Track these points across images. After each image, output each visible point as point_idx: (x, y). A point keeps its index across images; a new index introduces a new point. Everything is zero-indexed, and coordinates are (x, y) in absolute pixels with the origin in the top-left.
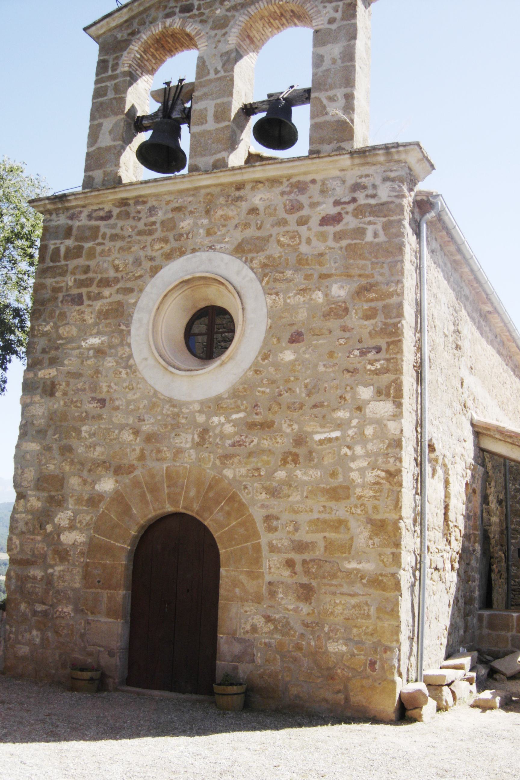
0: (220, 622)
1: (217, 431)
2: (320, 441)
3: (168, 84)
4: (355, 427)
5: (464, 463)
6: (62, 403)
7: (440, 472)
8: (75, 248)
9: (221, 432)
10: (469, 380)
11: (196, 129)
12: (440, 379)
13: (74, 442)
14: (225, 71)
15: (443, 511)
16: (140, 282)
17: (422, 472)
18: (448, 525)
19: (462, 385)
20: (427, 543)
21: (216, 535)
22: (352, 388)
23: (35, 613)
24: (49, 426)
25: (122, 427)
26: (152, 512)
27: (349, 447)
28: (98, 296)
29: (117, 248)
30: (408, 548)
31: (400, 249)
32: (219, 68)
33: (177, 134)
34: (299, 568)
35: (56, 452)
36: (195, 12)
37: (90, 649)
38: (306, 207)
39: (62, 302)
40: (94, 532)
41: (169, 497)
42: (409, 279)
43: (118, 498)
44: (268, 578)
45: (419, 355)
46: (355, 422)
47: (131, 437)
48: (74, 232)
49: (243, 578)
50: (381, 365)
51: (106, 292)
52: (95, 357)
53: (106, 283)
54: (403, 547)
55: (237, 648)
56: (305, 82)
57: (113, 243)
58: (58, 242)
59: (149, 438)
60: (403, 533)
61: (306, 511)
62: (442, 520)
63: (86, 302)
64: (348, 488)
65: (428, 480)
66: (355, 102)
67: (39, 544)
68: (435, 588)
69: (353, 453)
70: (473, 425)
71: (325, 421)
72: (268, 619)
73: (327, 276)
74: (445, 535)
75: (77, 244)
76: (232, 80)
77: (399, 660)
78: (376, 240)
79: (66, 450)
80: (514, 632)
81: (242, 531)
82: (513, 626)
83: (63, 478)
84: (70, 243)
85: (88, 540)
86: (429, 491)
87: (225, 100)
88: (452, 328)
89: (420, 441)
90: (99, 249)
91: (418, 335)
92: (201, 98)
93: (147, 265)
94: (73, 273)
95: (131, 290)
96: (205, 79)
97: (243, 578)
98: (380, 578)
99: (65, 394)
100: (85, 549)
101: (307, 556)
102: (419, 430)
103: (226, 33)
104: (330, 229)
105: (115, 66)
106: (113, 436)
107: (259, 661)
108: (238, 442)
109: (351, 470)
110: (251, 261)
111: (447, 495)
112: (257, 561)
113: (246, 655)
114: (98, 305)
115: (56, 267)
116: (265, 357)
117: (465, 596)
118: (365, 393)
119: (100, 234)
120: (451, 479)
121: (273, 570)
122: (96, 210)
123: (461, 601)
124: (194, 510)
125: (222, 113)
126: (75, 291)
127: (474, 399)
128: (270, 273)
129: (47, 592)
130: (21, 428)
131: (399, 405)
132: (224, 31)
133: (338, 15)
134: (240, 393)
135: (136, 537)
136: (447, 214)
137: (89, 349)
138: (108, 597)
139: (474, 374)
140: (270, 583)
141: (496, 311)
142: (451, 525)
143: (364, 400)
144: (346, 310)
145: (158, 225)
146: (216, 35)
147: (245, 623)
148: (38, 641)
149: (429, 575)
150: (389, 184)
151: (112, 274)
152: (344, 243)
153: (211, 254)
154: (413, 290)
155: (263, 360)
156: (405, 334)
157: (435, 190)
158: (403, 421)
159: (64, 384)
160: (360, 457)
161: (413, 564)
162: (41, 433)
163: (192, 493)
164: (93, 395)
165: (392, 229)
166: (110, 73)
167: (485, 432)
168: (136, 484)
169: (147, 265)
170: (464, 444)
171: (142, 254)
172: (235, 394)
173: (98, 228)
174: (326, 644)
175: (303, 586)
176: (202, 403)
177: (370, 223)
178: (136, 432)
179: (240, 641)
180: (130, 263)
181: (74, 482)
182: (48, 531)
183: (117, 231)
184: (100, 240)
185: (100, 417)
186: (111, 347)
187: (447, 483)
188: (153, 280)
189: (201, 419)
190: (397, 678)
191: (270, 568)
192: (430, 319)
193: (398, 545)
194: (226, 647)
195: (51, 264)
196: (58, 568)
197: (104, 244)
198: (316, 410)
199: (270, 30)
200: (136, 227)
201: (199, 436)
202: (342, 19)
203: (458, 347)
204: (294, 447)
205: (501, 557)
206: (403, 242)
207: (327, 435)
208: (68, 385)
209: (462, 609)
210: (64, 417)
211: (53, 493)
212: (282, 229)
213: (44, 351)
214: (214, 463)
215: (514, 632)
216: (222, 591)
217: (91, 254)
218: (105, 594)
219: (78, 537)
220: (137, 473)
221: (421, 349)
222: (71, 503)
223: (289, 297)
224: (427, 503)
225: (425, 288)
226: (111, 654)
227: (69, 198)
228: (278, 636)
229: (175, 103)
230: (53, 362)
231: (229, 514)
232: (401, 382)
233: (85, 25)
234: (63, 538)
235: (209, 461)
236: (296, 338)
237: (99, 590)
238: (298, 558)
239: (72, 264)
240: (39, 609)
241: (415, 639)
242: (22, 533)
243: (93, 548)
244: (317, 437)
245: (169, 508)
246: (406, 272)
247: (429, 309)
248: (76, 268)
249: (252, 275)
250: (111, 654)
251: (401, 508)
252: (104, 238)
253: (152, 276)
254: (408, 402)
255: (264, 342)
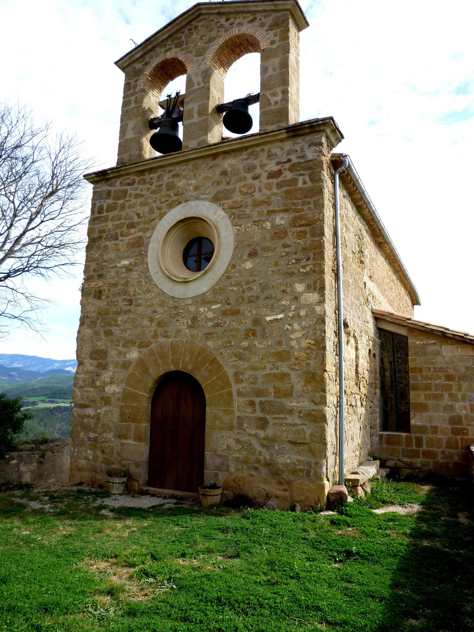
0: (206, 444)
1: (203, 317)
2: (270, 321)
3: (169, 96)
4: (293, 311)
5: (367, 337)
6: (106, 303)
7: (352, 341)
8: (112, 204)
9: (206, 317)
10: (370, 284)
11: (187, 122)
12: (350, 281)
13: (113, 329)
14: (204, 83)
15: (355, 368)
16: (153, 223)
17: (340, 342)
18: (358, 377)
19: (365, 287)
20: (344, 388)
21: (203, 386)
22: (290, 285)
23: (89, 439)
24: (98, 319)
25: (143, 317)
26: (162, 371)
27: (290, 325)
28: (128, 234)
29: (138, 203)
30: (331, 392)
31: (320, 191)
32: (201, 81)
33: (176, 128)
34: (257, 407)
35: (102, 336)
36: (184, 46)
37: (124, 462)
38: (258, 167)
39: (105, 239)
40: (126, 385)
41: (173, 362)
42: (328, 211)
43: (141, 363)
44: (237, 414)
45: (335, 263)
46: (293, 307)
47: (148, 324)
48: (112, 194)
49: (221, 414)
50: (310, 268)
51: (132, 231)
52: (126, 273)
53: (132, 226)
54: (327, 391)
55: (218, 461)
56: (256, 90)
57: (136, 200)
58: (102, 201)
59: (159, 324)
60: (328, 382)
61: (262, 368)
62: (354, 374)
63: (120, 238)
64: (289, 352)
65: (344, 346)
66: (289, 95)
67: (92, 393)
68: (350, 418)
69: (293, 328)
70: (373, 313)
71: (272, 309)
72: (238, 441)
73: (273, 212)
74: (357, 384)
75: (114, 201)
76: (209, 89)
77: (327, 469)
78: (305, 186)
79: (108, 333)
80: (403, 447)
81: (219, 382)
82: (403, 442)
83: (106, 352)
84: (110, 201)
85: (122, 391)
86: (344, 354)
87: (205, 102)
88: (358, 249)
89: (338, 321)
90: (127, 204)
91: (335, 250)
92: (189, 102)
93: (157, 212)
94: (112, 220)
95: (148, 229)
96: (191, 89)
97: (221, 414)
98: (313, 413)
99: (108, 297)
100: (120, 396)
101: (263, 399)
102: (337, 312)
103: (204, 58)
104: (275, 181)
105: (135, 87)
106: (137, 323)
107: (232, 470)
108: (217, 323)
109: (291, 339)
110: (223, 205)
111: (357, 357)
112: (230, 402)
113: (223, 467)
114: (127, 239)
115: (101, 217)
116: (234, 266)
117: (371, 423)
118: (300, 287)
119: (128, 194)
120: (359, 347)
121: (240, 408)
122: (125, 179)
123: (368, 427)
124: (189, 369)
125: (203, 110)
126: (113, 232)
127: (373, 297)
128: (236, 213)
129: (96, 425)
130: (80, 320)
131: (323, 295)
132: (202, 57)
133: (277, 38)
134: (216, 290)
135: (152, 388)
136: (352, 170)
137: (121, 268)
138: (135, 428)
139: (373, 281)
140: (238, 417)
141: (386, 242)
142: (360, 376)
143: (299, 292)
144: (286, 233)
145: (164, 186)
146: (198, 60)
147: (223, 444)
148: (91, 457)
149: (346, 410)
150: (313, 148)
151: (136, 219)
152: (284, 189)
153: (198, 202)
154: (331, 219)
155: (232, 269)
156: (326, 247)
157: (345, 152)
158: (325, 305)
159: (107, 291)
160: (296, 331)
161: (335, 402)
162: (93, 324)
163: (187, 359)
164: (125, 297)
165: (317, 179)
166: (132, 91)
167: (380, 317)
168: (152, 353)
169: (157, 212)
170: (367, 325)
171: (154, 205)
172: (214, 290)
173: (126, 191)
174: (276, 458)
175: (260, 419)
176: (192, 298)
177: (301, 175)
178: (151, 320)
179: (220, 456)
180: (147, 212)
181: (113, 353)
182: (98, 385)
183: (138, 192)
184: (128, 198)
185: (129, 311)
186: (136, 265)
187: (357, 349)
188: (161, 221)
189: (192, 309)
190: (326, 482)
191: (238, 407)
192: (343, 240)
193: (324, 391)
194: (210, 460)
195: (98, 215)
196: (104, 409)
197: (130, 200)
198: (267, 301)
199: (234, 56)
200: (150, 189)
201: (191, 321)
202: (279, 41)
203: (362, 262)
204: (253, 326)
205: (392, 397)
206: (323, 186)
207: (275, 317)
208: (109, 291)
209: (369, 431)
210: (107, 313)
211: (100, 361)
212: (242, 183)
213: (94, 270)
214: (201, 338)
215: (403, 447)
216: (207, 423)
217: (123, 208)
218: (133, 425)
219: (116, 389)
220: (153, 346)
221: (337, 258)
222: (111, 368)
223: (248, 227)
224: (343, 362)
225: (340, 218)
226: (137, 465)
227: (108, 172)
228: (244, 453)
229: (174, 106)
230: (101, 276)
231: (211, 371)
232: (324, 279)
233: (115, 61)
234: (106, 389)
235: (199, 337)
236: (253, 255)
237: (130, 424)
238: (257, 400)
239: (111, 214)
240: (92, 437)
241: (338, 454)
242: (82, 387)
243: (126, 396)
244: (268, 319)
245: (172, 368)
246: (325, 206)
247: (342, 233)
248: (113, 217)
249: (223, 214)
250: (137, 465)
251: (325, 365)
252: (130, 197)
253: (160, 219)
254: (329, 292)
255: (232, 257)
